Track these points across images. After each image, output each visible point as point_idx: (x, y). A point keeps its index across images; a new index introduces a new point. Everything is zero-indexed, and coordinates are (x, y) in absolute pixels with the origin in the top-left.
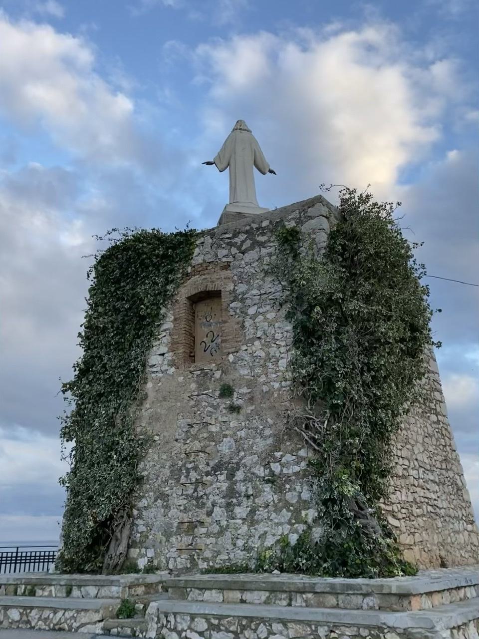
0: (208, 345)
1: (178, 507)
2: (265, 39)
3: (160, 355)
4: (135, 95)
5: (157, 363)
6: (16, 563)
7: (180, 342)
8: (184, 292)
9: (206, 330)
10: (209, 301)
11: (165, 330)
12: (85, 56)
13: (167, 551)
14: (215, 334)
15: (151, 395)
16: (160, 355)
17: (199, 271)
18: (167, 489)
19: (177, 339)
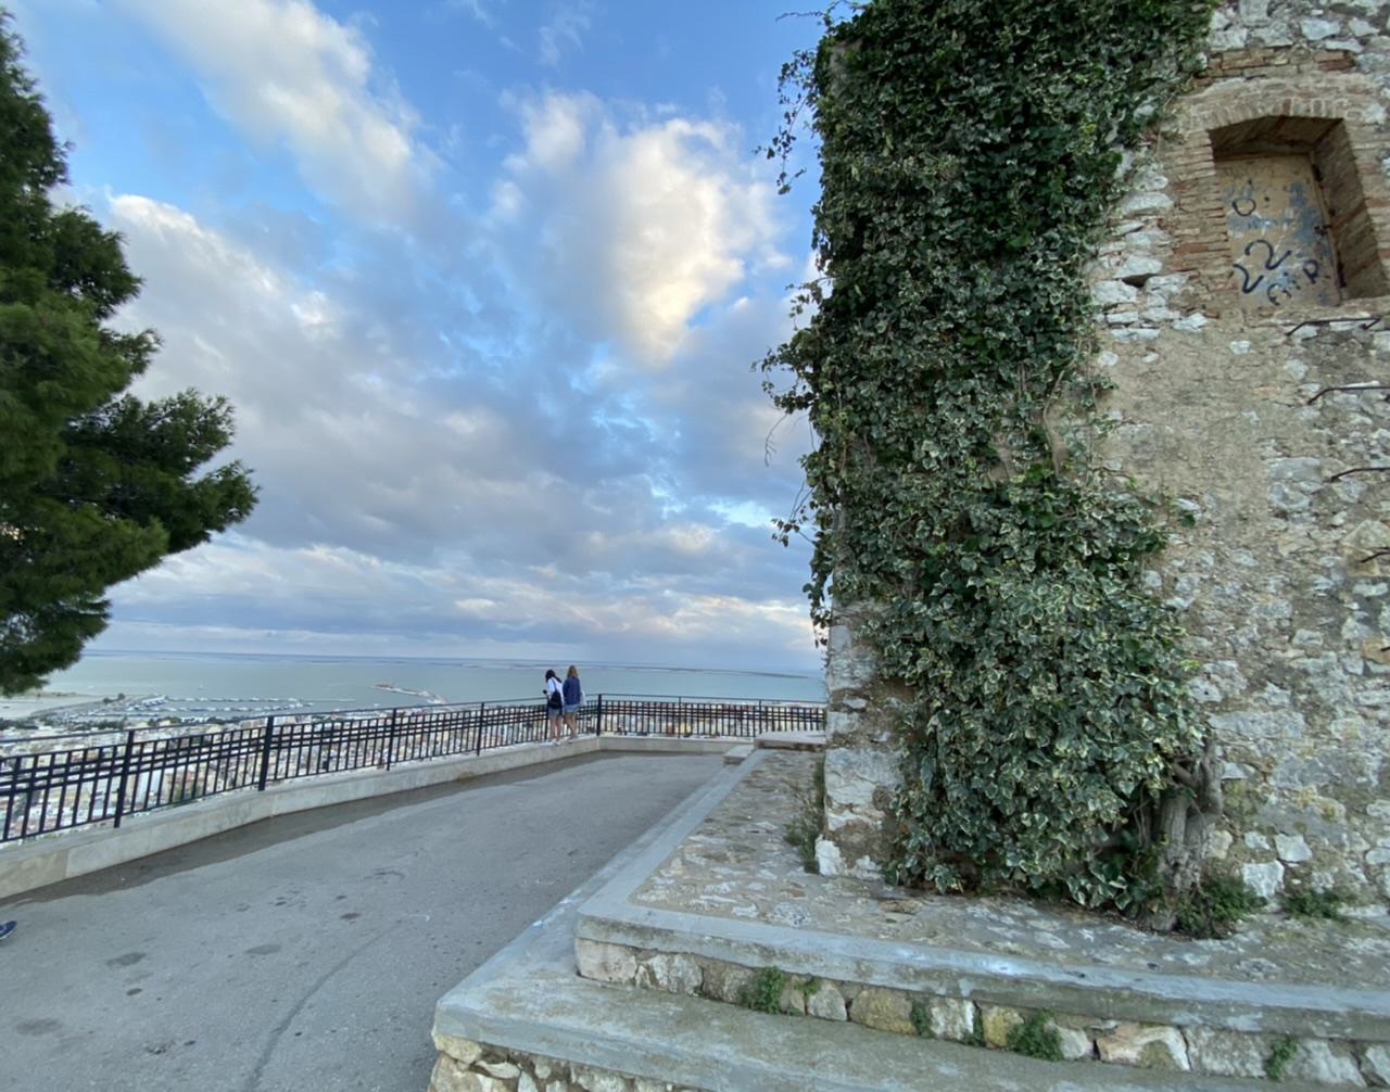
0: (1254, 276)
1: (1369, 713)
2: (588, 100)
3: (1129, 281)
4: (417, 137)
5: (1123, 299)
6: (392, 737)
7: (1211, 247)
8: (1200, 114)
9: (1240, 235)
10: (1243, 163)
11: (1137, 215)
12: (356, 61)
13: (1365, 846)
14: (1276, 248)
15: (1127, 388)
16: (1129, 281)
17: (1242, 68)
18: (1291, 653)
19: (1196, 236)
